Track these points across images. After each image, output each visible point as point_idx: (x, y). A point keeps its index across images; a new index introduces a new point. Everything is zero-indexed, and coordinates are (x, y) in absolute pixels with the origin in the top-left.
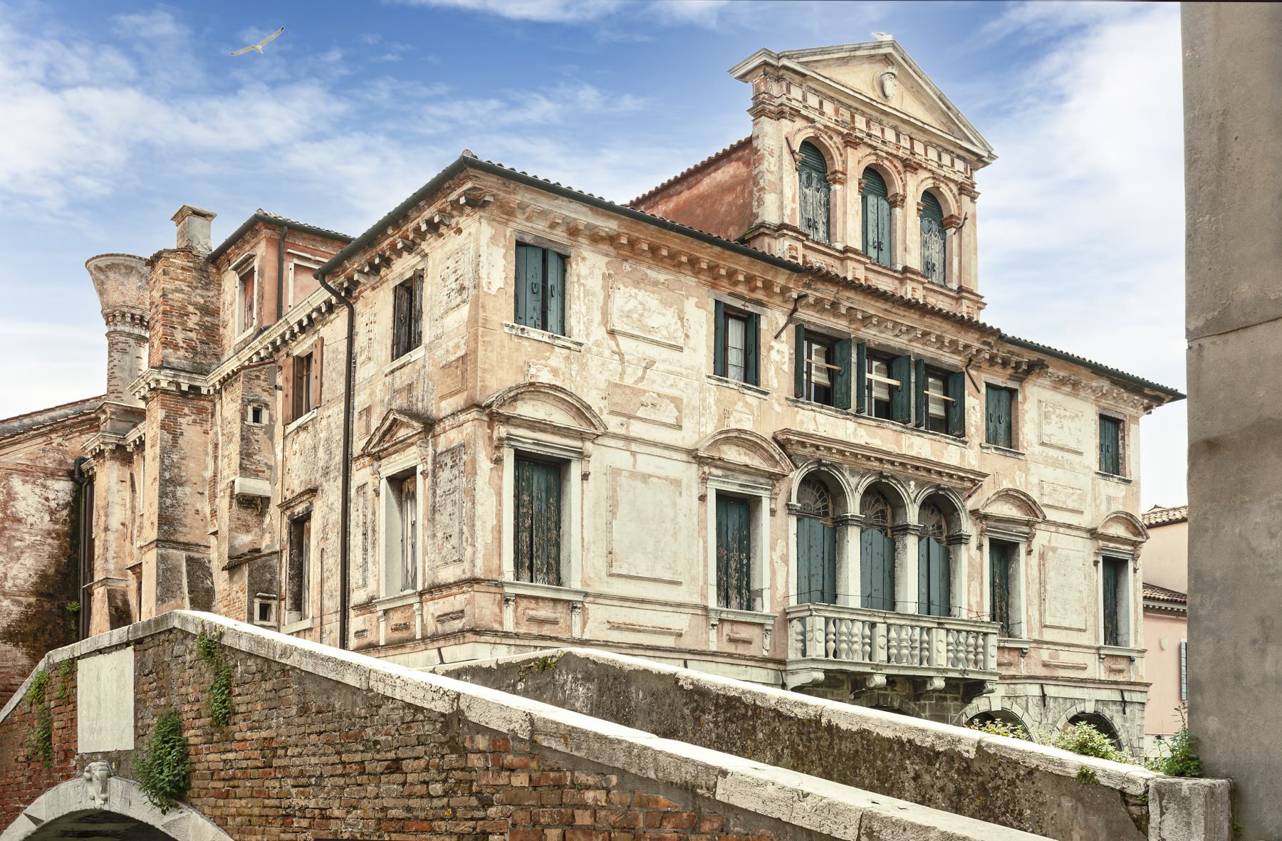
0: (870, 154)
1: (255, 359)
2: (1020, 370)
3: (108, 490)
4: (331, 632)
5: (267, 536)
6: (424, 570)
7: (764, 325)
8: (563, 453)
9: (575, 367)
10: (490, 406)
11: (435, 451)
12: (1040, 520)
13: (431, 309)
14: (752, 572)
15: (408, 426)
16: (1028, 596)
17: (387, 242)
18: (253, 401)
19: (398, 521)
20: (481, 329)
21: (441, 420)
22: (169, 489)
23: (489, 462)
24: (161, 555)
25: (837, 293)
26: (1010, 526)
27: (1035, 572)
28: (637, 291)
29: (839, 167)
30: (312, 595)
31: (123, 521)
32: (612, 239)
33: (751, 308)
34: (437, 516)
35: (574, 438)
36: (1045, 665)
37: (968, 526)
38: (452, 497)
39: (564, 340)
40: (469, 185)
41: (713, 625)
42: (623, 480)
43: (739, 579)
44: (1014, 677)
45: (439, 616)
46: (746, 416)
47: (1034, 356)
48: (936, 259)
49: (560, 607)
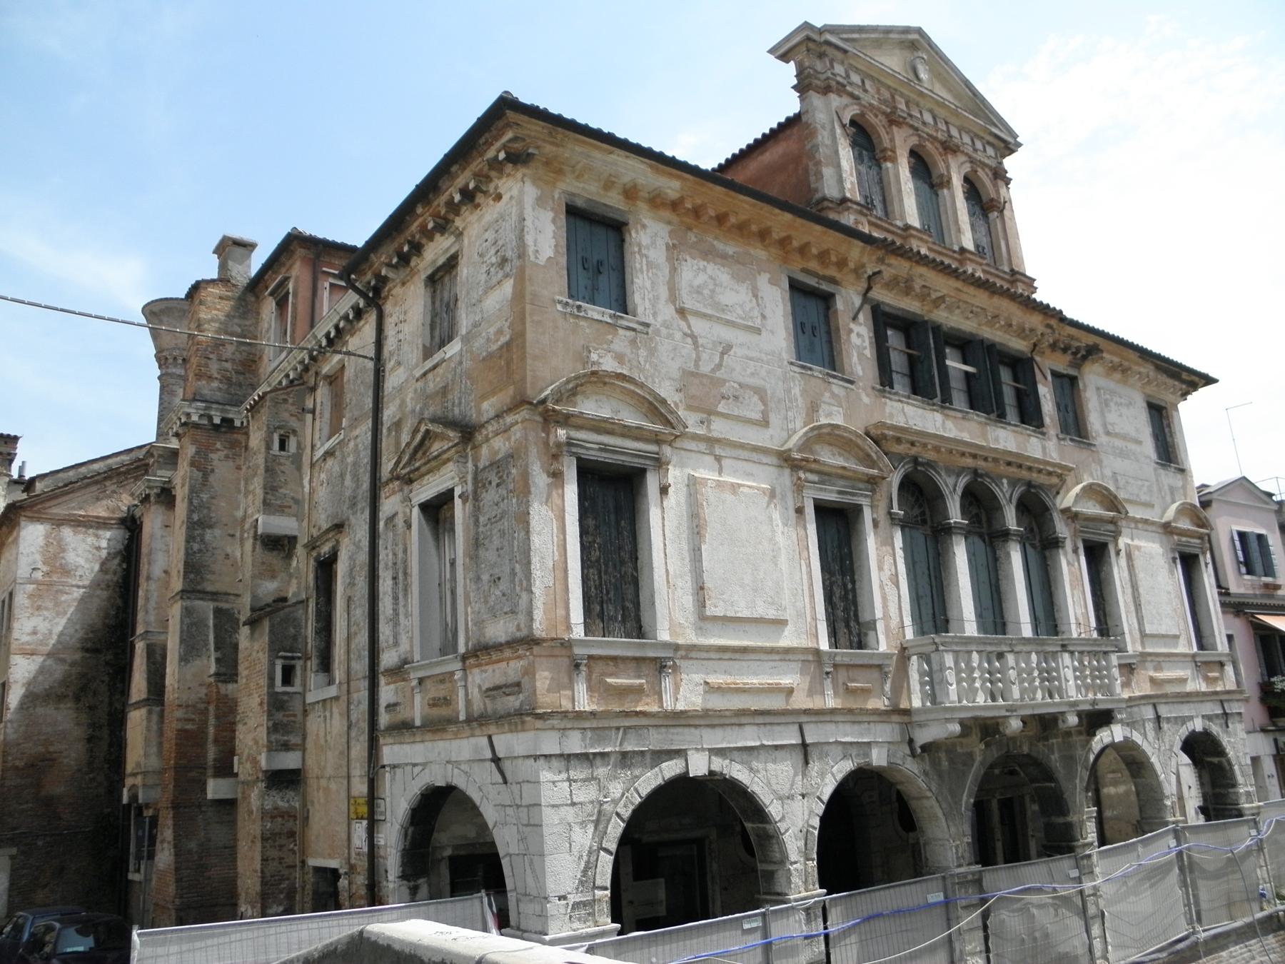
1: (284, 383)
2: (1079, 356)
3: (152, 536)
4: (359, 703)
5: (294, 581)
6: (467, 624)
7: (840, 304)
8: (636, 460)
9: (643, 353)
10: (543, 402)
11: (476, 466)
13: (468, 293)
14: (859, 599)
15: (443, 437)
17: (416, 224)
18: (279, 427)
19: (435, 560)
20: (528, 307)
21: (482, 426)
22: (197, 532)
23: (545, 476)
24: (186, 608)
25: (910, 269)
28: (705, 263)
29: (887, 144)
30: (339, 652)
31: (165, 568)
32: (675, 205)
33: (825, 287)
34: (482, 552)
35: (647, 441)
37: (1062, 529)
38: (499, 525)
39: (628, 320)
40: (509, 135)
41: (827, 673)
43: (846, 610)
45: (489, 690)
46: (836, 408)
48: (984, 242)
49: (646, 669)
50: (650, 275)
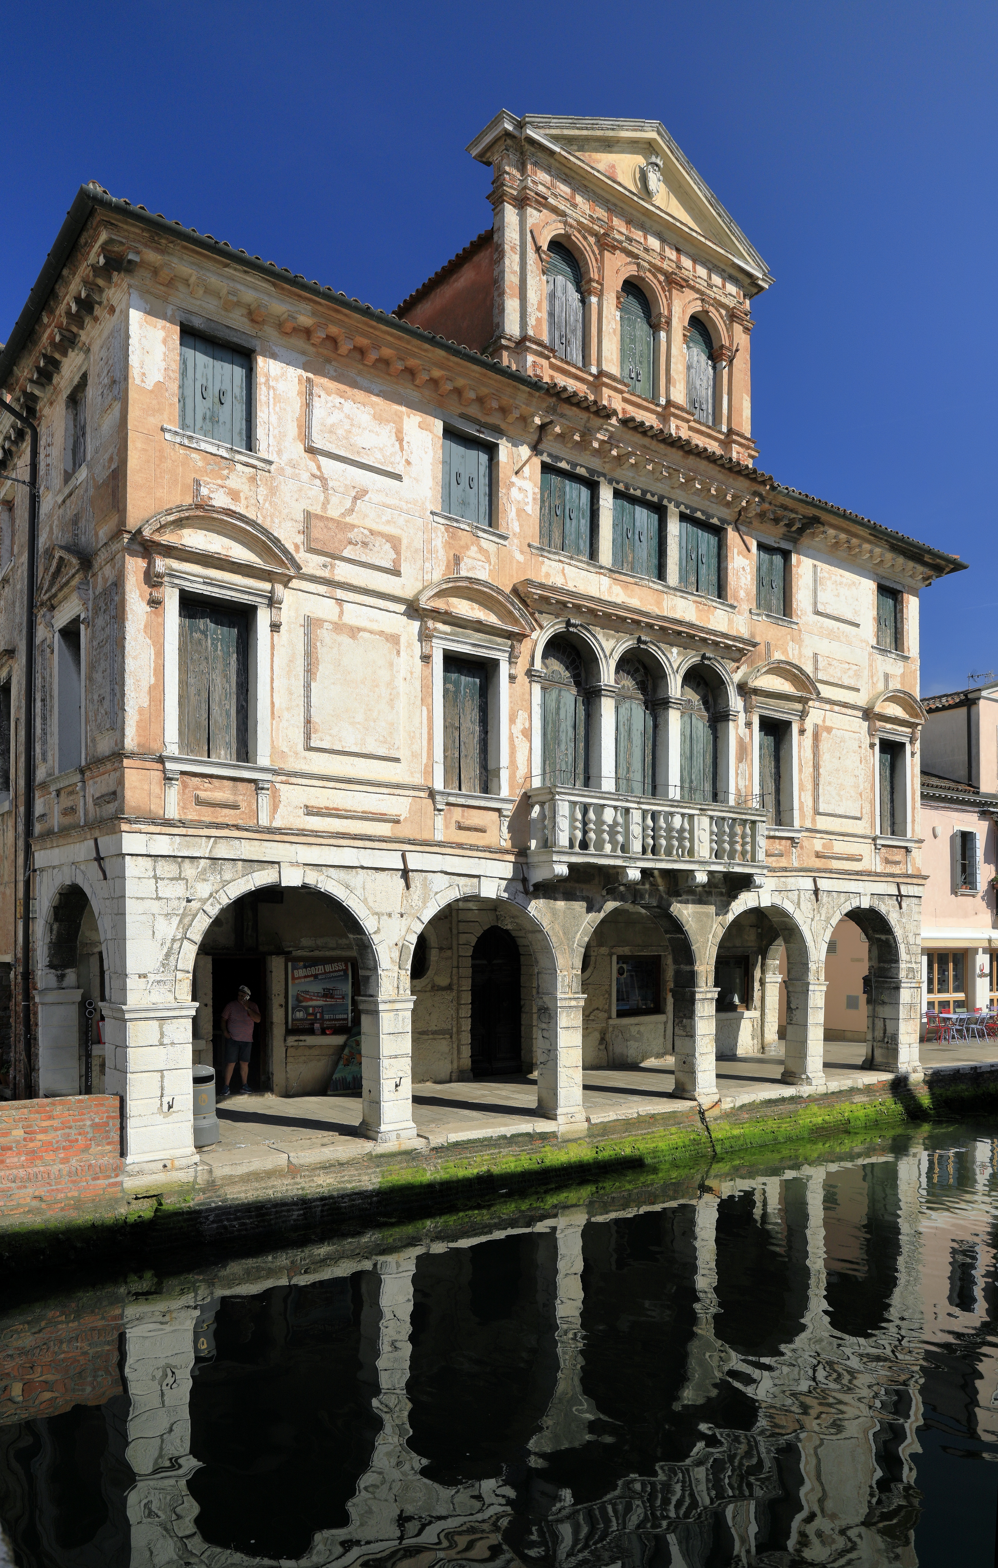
0: (630, 263)
2: (794, 529)
8: (246, 597)
9: (263, 491)
12: (814, 697)
16: (801, 780)
26: (782, 703)
27: (808, 754)
28: (342, 401)
36: (818, 855)
37: (736, 702)
42: (325, 634)
44: (785, 869)
46: (480, 563)
47: (811, 511)
48: (705, 392)
50: (277, 409)
